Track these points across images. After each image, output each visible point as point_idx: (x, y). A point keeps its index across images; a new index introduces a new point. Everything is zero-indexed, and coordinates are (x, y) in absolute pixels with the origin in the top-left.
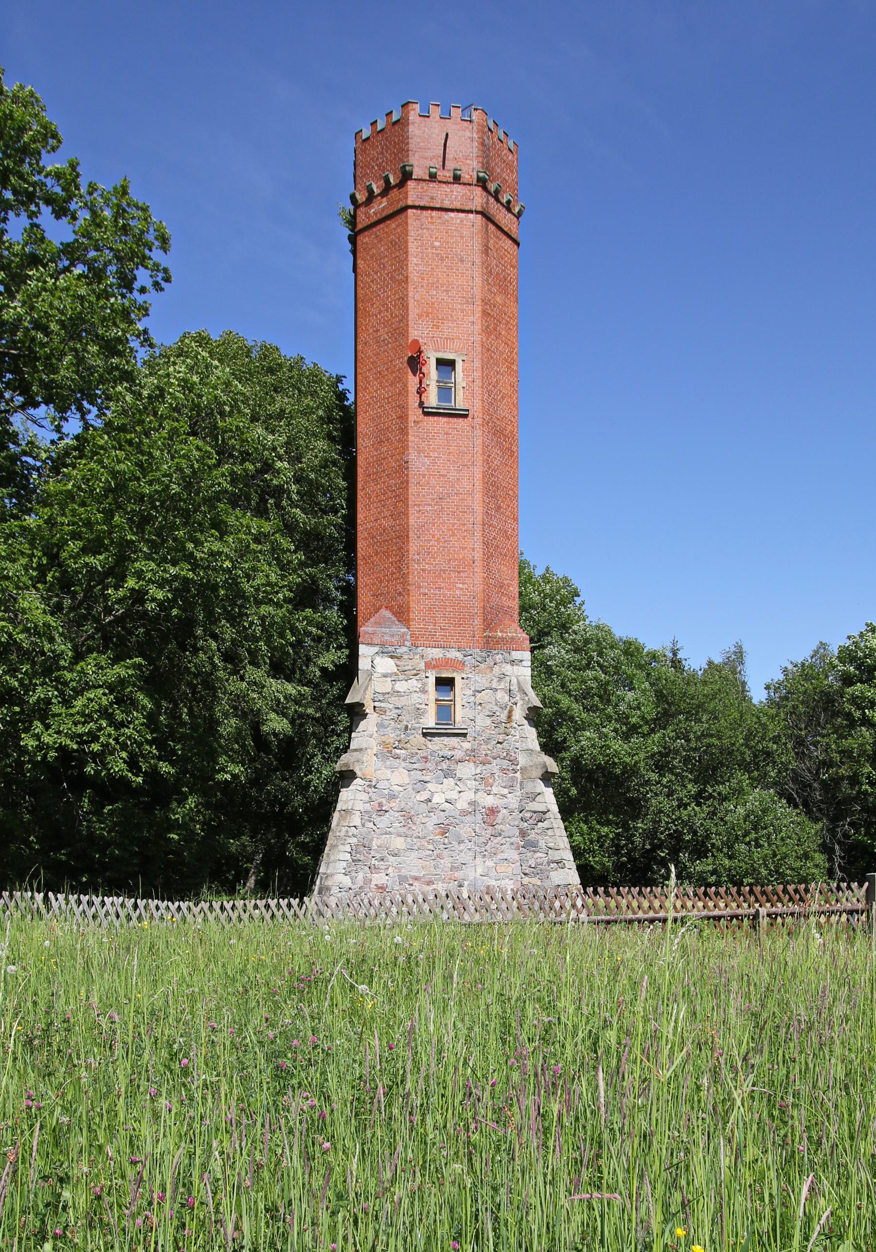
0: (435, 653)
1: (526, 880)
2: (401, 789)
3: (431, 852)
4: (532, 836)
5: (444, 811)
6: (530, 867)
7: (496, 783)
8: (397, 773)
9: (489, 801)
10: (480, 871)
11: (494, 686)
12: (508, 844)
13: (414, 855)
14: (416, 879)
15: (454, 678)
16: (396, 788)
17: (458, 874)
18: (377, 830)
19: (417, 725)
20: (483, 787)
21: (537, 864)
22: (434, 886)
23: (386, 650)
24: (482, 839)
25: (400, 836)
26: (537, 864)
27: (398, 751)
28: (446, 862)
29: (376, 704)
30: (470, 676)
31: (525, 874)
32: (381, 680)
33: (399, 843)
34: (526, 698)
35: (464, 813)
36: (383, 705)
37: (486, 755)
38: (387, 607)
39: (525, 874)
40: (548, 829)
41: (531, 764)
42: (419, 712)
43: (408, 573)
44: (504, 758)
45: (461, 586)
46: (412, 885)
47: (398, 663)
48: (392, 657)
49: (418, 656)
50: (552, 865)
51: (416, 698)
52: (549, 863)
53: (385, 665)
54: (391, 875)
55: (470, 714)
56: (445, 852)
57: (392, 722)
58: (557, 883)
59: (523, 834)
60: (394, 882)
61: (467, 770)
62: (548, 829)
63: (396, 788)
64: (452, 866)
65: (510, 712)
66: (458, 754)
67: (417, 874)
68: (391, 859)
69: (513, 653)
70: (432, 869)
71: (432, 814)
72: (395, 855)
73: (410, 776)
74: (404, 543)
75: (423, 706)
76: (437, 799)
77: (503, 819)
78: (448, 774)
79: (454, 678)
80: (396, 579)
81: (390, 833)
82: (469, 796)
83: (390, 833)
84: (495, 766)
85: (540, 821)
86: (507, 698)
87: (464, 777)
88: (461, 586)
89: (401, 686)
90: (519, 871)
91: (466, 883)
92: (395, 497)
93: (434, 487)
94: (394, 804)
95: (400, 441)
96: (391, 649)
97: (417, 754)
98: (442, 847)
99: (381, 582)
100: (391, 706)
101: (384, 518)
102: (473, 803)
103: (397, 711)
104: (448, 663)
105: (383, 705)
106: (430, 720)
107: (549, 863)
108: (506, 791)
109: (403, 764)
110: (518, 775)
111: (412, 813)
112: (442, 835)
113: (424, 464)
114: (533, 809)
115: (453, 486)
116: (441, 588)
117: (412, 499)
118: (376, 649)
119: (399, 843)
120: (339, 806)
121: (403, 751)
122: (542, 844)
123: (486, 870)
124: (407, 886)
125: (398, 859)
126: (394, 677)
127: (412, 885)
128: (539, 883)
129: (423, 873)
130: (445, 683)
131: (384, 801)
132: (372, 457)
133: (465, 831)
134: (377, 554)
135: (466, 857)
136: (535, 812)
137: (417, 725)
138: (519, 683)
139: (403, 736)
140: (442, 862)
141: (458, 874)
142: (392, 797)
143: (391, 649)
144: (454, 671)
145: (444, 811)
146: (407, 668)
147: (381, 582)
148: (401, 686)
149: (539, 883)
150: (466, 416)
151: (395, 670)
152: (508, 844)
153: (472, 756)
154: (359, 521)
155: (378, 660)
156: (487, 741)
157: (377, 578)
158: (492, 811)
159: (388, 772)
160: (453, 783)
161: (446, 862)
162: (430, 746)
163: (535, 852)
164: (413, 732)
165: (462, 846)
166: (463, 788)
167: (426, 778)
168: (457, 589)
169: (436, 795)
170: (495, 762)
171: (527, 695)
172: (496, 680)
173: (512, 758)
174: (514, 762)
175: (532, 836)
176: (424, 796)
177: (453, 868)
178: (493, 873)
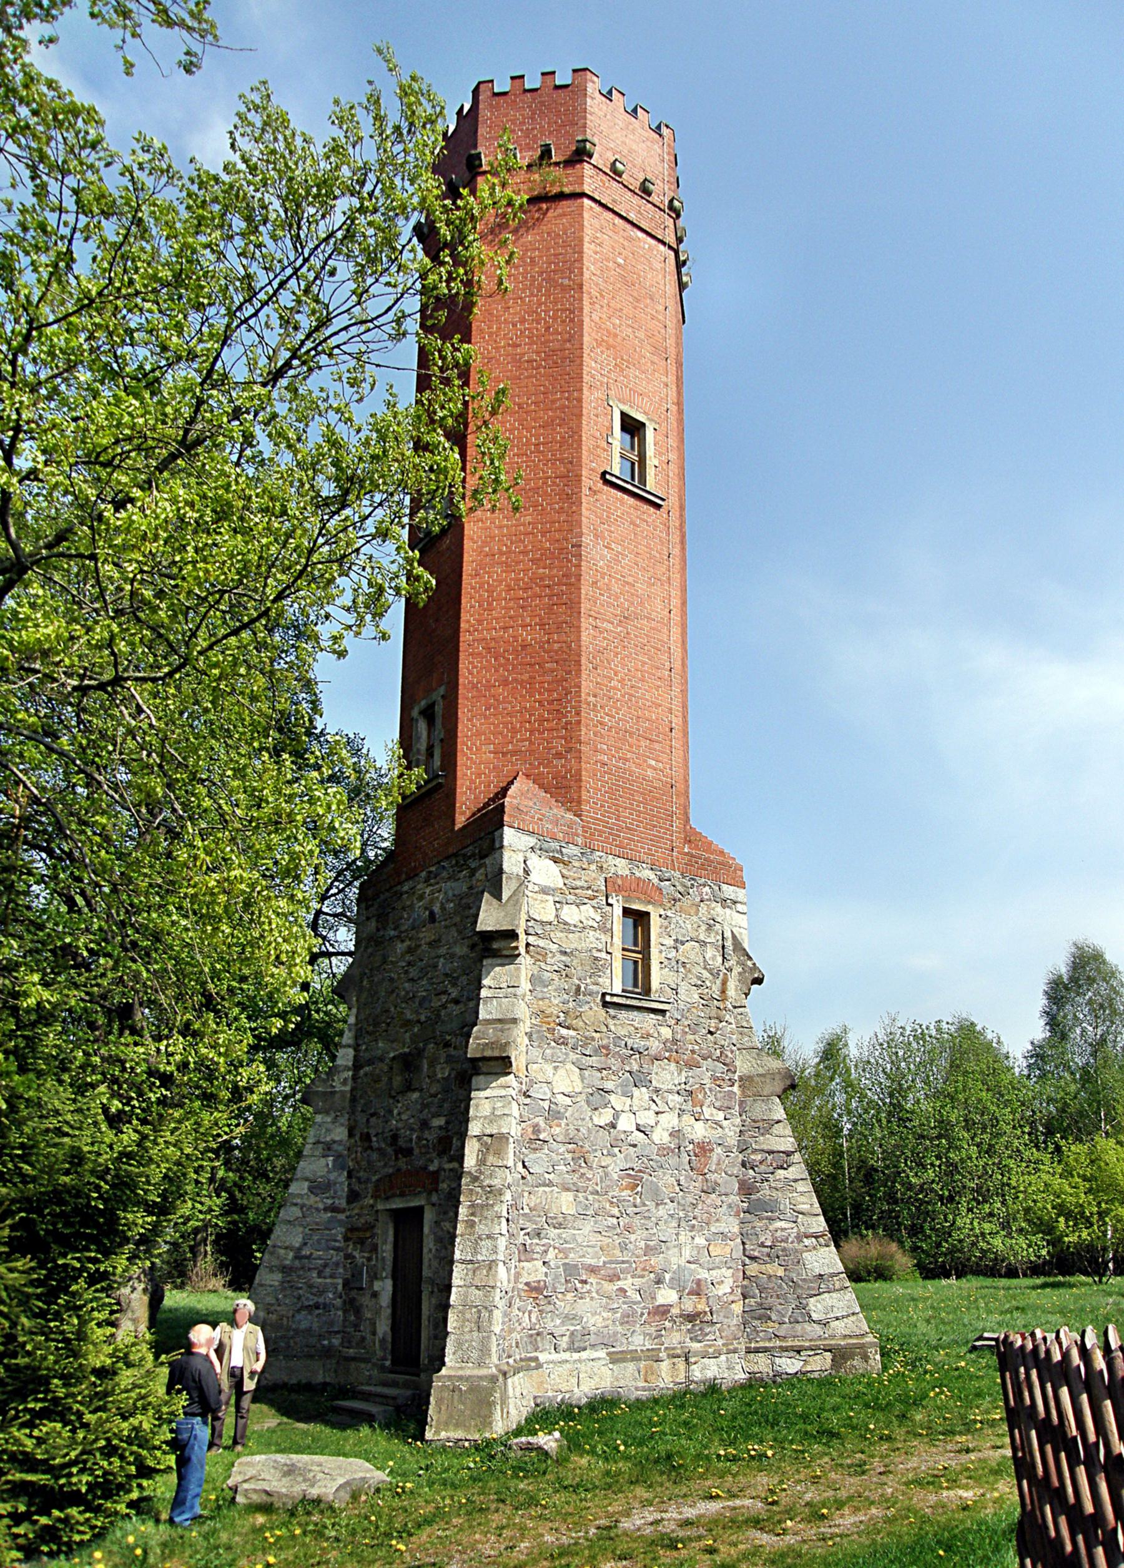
0: (621, 867)
1: (753, 1269)
2: (568, 1101)
3: (615, 1221)
4: (765, 1192)
5: (635, 1146)
6: (762, 1245)
7: (708, 1102)
8: (561, 1072)
9: (699, 1131)
10: (687, 1253)
11: (702, 937)
12: (725, 1207)
13: (588, 1226)
14: (593, 1270)
15: (648, 914)
16: (561, 1099)
17: (655, 1261)
18: (529, 1177)
19: (594, 988)
20: (690, 1108)
21: (775, 1240)
22: (620, 1284)
23: (545, 846)
24: (690, 1199)
25: (568, 1190)
26: (775, 1240)
27: (564, 1032)
28: (637, 1239)
29: (531, 939)
30: (669, 913)
31: (753, 1258)
32: (539, 896)
33: (566, 1203)
34: (749, 963)
35: (664, 1151)
36: (541, 943)
37: (693, 1052)
38: (528, 776)
39: (753, 1258)
40: (796, 1181)
41: (761, 1071)
42: (597, 966)
43: (579, 722)
44: (718, 1060)
45: (653, 763)
46: (585, 1282)
47: (565, 872)
48: (555, 861)
49: (593, 867)
50: (807, 1242)
51: (593, 939)
52: (799, 1238)
53: (545, 872)
54: (552, 1264)
55: (672, 979)
56: (637, 1221)
57: (555, 976)
58: (817, 1272)
59: (746, 1189)
60: (557, 1277)
61: (667, 1076)
62: (796, 1181)
63: (561, 1099)
64: (647, 1246)
65: (724, 983)
66: (655, 1046)
67: (593, 1262)
68: (553, 1232)
69: (724, 887)
70: (617, 1252)
71: (616, 1150)
72: (559, 1226)
73: (582, 1078)
74: (569, 672)
75: (603, 955)
76: (626, 1123)
77: (718, 1164)
78: (640, 1080)
79: (648, 914)
80: (551, 730)
81: (550, 1184)
82: (669, 1120)
83: (550, 1184)
84: (705, 1073)
85: (782, 1168)
86: (720, 959)
87: (664, 1087)
88: (653, 763)
89: (570, 914)
90: (738, 1253)
91: (667, 1276)
92: (550, 597)
93: (617, 598)
94: (558, 1130)
95: (561, 510)
96: (555, 845)
97: (593, 1039)
98: (631, 1210)
99: (514, 731)
100: (554, 947)
101: (524, 626)
102: (676, 1134)
103: (564, 958)
104: (636, 887)
105: (541, 943)
106: (616, 982)
107: (799, 1238)
108: (720, 1116)
109: (573, 1056)
110: (736, 1089)
111: (587, 1147)
112: (632, 1189)
113: (602, 558)
114: (765, 1147)
115: (642, 603)
116: (626, 760)
117: (585, 606)
118: (532, 841)
119: (566, 1203)
120: (474, 1128)
121: (572, 1033)
122: (785, 1205)
123: (695, 1253)
124: (579, 1285)
125: (566, 1234)
126: (561, 897)
127: (585, 1282)
128: (780, 1272)
129: (603, 1258)
130: (638, 919)
131: (541, 1121)
132: (500, 527)
133: (666, 1181)
134: (505, 683)
135: (667, 1231)
136: (770, 1152)
137: (594, 988)
138: (734, 936)
139: (571, 1005)
140: (633, 1237)
141: (655, 1261)
142: (554, 1115)
143: (555, 845)
144: (649, 902)
145: (635, 1146)
146: (579, 883)
147: (514, 731)
148: (570, 914)
149: (780, 1272)
150: (658, 507)
151: (560, 883)
152: (725, 1207)
153: (673, 1050)
154: (463, 625)
155: (534, 861)
156: (693, 1028)
157: (505, 724)
158: (703, 1149)
159: (549, 1068)
160: (646, 1097)
161: (637, 1239)
162: (613, 1028)
163: (770, 1219)
164: (588, 998)
165: (662, 1212)
166: (662, 1107)
167: (609, 1085)
168: (650, 766)
169: (623, 1117)
170: (705, 1064)
171: (750, 958)
172: (704, 927)
173: (728, 1061)
174: (730, 1068)
175: (765, 1192)
176: (604, 1117)
177: (648, 1250)
178: (705, 1259)
